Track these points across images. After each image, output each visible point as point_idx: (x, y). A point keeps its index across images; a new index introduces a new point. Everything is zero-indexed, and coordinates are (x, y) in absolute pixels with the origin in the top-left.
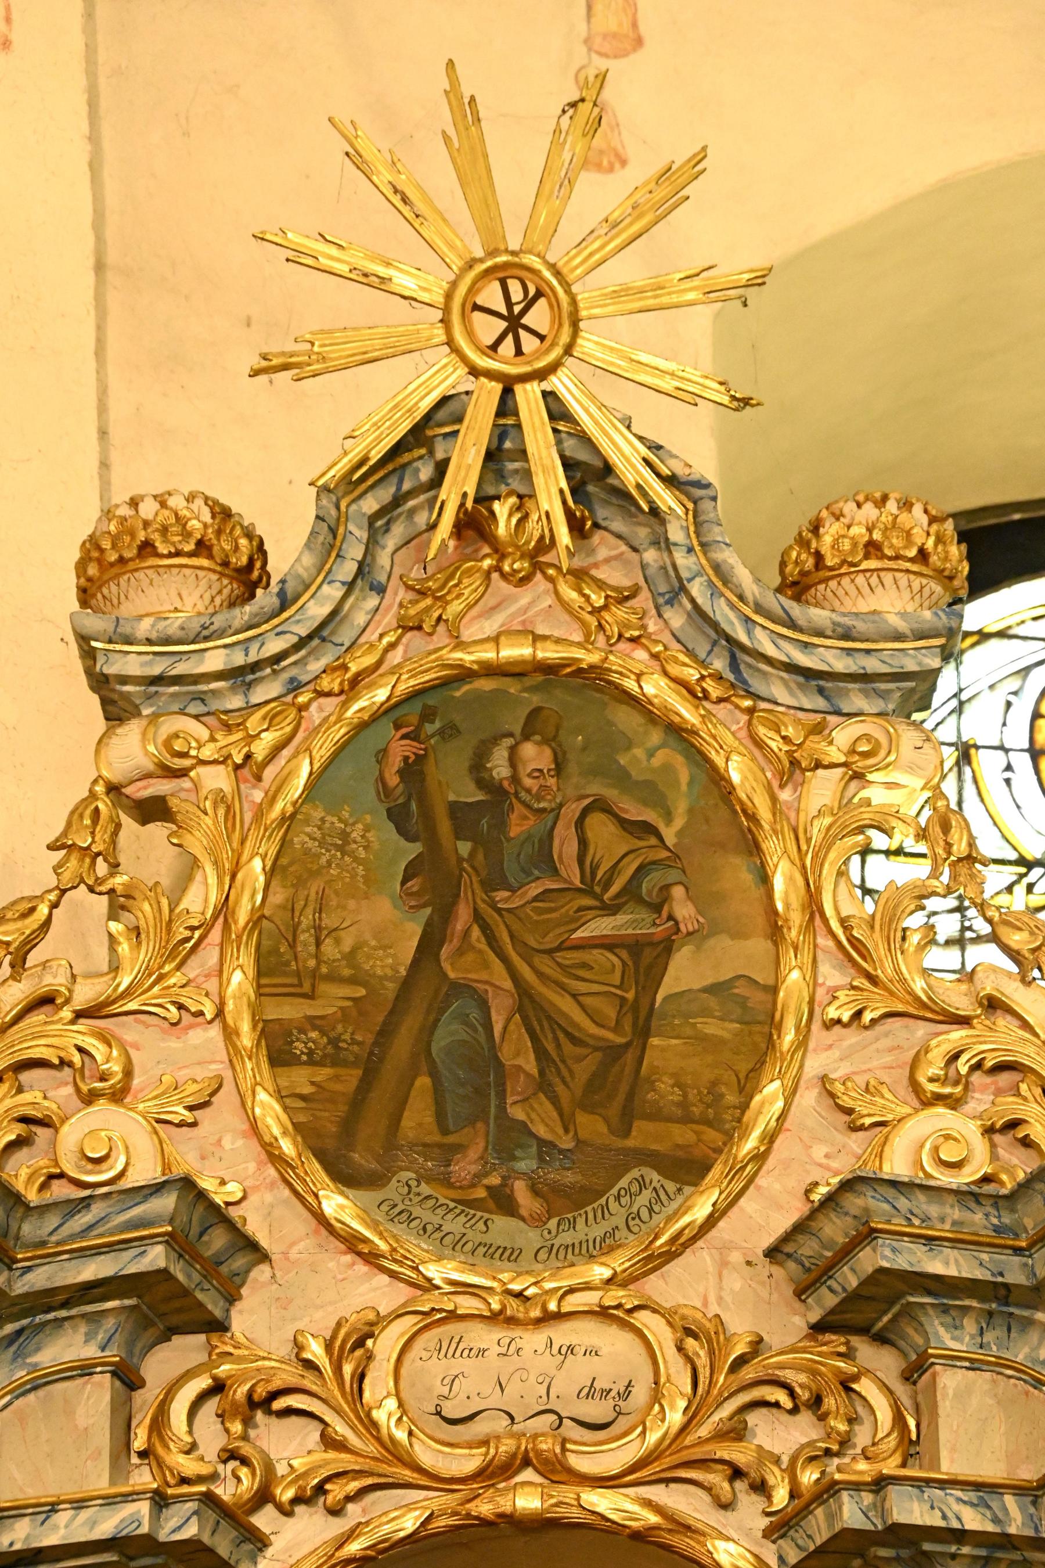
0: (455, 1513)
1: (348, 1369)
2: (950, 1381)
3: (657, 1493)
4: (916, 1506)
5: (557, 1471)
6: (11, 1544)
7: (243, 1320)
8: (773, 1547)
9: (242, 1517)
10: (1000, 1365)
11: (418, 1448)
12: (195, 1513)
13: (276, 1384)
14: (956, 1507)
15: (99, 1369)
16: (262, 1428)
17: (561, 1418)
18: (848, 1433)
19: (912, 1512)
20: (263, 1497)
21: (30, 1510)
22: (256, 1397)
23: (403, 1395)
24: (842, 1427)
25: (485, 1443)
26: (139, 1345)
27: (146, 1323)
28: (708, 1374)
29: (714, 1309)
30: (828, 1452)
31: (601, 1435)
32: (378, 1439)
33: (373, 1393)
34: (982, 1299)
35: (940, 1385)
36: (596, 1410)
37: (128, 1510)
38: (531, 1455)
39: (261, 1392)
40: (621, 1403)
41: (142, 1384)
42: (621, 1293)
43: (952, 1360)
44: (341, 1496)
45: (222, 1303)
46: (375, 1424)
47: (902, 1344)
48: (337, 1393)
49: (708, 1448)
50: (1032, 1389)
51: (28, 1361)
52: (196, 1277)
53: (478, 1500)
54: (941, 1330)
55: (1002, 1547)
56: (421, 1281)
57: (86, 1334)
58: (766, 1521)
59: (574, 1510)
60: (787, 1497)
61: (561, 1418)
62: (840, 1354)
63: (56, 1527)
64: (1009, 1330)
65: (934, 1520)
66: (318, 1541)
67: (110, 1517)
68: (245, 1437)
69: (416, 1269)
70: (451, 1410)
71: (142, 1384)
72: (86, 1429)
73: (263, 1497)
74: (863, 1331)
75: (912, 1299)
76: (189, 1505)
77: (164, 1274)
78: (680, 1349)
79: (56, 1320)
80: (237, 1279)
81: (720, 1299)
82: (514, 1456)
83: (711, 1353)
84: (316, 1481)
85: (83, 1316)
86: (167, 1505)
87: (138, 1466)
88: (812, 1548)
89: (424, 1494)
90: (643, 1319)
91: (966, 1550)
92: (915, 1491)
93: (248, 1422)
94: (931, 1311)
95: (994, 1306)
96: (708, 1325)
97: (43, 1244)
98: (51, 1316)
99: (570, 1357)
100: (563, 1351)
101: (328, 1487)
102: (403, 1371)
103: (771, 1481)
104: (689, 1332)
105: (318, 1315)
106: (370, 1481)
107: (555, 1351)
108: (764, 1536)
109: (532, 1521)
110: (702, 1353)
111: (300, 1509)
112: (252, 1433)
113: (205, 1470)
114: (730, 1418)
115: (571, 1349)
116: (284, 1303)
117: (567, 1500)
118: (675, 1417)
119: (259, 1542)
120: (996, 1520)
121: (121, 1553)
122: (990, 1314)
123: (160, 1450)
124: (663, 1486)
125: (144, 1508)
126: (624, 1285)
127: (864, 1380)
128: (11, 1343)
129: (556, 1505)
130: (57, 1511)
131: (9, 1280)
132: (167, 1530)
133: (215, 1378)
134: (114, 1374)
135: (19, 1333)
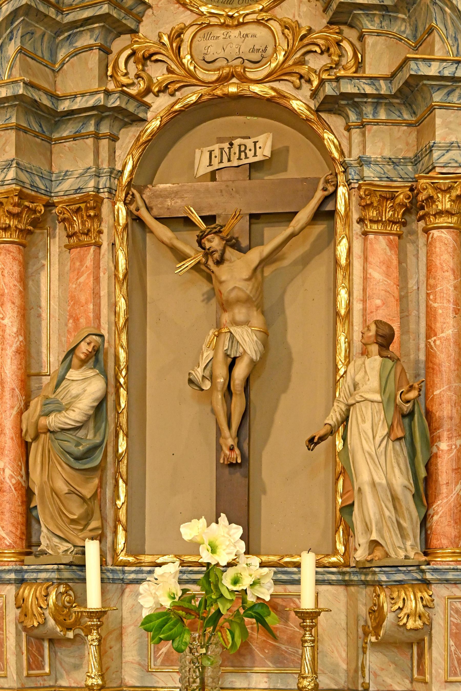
0: (209, 94)
1: (174, 45)
2: (370, 40)
3: (276, 85)
4: (349, 86)
5: (243, 79)
7: (144, 30)
8: (313, 101)
10: (386, 35)
11: (197, 72)
12: (119, 97)
13: (152, 51)
14: (363, 86)
16: (149, 67)
17: (244, 60)
18: (339, 61)
20: (148, 91)
22: (145, 56)
23: (193, 54)
24: (336, 59)
26: (109, 39)
27: (109, 31)
30: (331, 68)
31: (257, 65)
34: (380, 11)
36: (255, 57)
37: (97, 96)
39: (147, 54)
41: (111, 52)
42: (264, 14)
43: (371, 33)
44: (173, 90)
48: (171, 53)
49: (291, 68)
52: (123, 15)
54: (367, 22)
56: (200, 13)
61: (244, 60)
62: (337, 33)
63: (76, 103)
64: (390, 21)
65: (356, 91)
68: (143, 70)
69: (198, 8)
70: (208, 59)
71: (111, 52)
73: (148, 91)
74: (345, 24)
75: (355, 12)
77: (108, 14)
80: (140, 15)
81: (299, 14)
82: (228, 74)
83: (293, 34)
85: (88, 29)
86: (110, 95)
87: (110, 81)
89: (201, 88)
90: (272, 24)
91: (370, 100)
92: (349, 81)
93: (144, 65)
94: (363, 16)
95: (384, 13)
96: (293, 24)
97: (71, 5)
98: (78, 30)
99: (247, 38)
101: (169, 86)
102: (193, 45)
103: (312, 79)
104: (286, 28)
105: (167, 26)
106: (182, 84)
109: (235, 96)
110: (290, 35)
111: (161, 94)
112: (146, 68)
113: (130, 81)
114: (299, 57)
115: (247, 35)
116: (156, 22)
118: (281, 58)
119: (148, 106)
120: (377, 89)
121: (98, 111)
122: (383, 16)
123: (115, 75)
125: (102, 96)
126: (266, 12)
127: (344, 41)
128: (68, 39)
129: (242, 90)
131: (62, 18)
133: (132, 50)
134: (99, 49)
135: (69, 36)
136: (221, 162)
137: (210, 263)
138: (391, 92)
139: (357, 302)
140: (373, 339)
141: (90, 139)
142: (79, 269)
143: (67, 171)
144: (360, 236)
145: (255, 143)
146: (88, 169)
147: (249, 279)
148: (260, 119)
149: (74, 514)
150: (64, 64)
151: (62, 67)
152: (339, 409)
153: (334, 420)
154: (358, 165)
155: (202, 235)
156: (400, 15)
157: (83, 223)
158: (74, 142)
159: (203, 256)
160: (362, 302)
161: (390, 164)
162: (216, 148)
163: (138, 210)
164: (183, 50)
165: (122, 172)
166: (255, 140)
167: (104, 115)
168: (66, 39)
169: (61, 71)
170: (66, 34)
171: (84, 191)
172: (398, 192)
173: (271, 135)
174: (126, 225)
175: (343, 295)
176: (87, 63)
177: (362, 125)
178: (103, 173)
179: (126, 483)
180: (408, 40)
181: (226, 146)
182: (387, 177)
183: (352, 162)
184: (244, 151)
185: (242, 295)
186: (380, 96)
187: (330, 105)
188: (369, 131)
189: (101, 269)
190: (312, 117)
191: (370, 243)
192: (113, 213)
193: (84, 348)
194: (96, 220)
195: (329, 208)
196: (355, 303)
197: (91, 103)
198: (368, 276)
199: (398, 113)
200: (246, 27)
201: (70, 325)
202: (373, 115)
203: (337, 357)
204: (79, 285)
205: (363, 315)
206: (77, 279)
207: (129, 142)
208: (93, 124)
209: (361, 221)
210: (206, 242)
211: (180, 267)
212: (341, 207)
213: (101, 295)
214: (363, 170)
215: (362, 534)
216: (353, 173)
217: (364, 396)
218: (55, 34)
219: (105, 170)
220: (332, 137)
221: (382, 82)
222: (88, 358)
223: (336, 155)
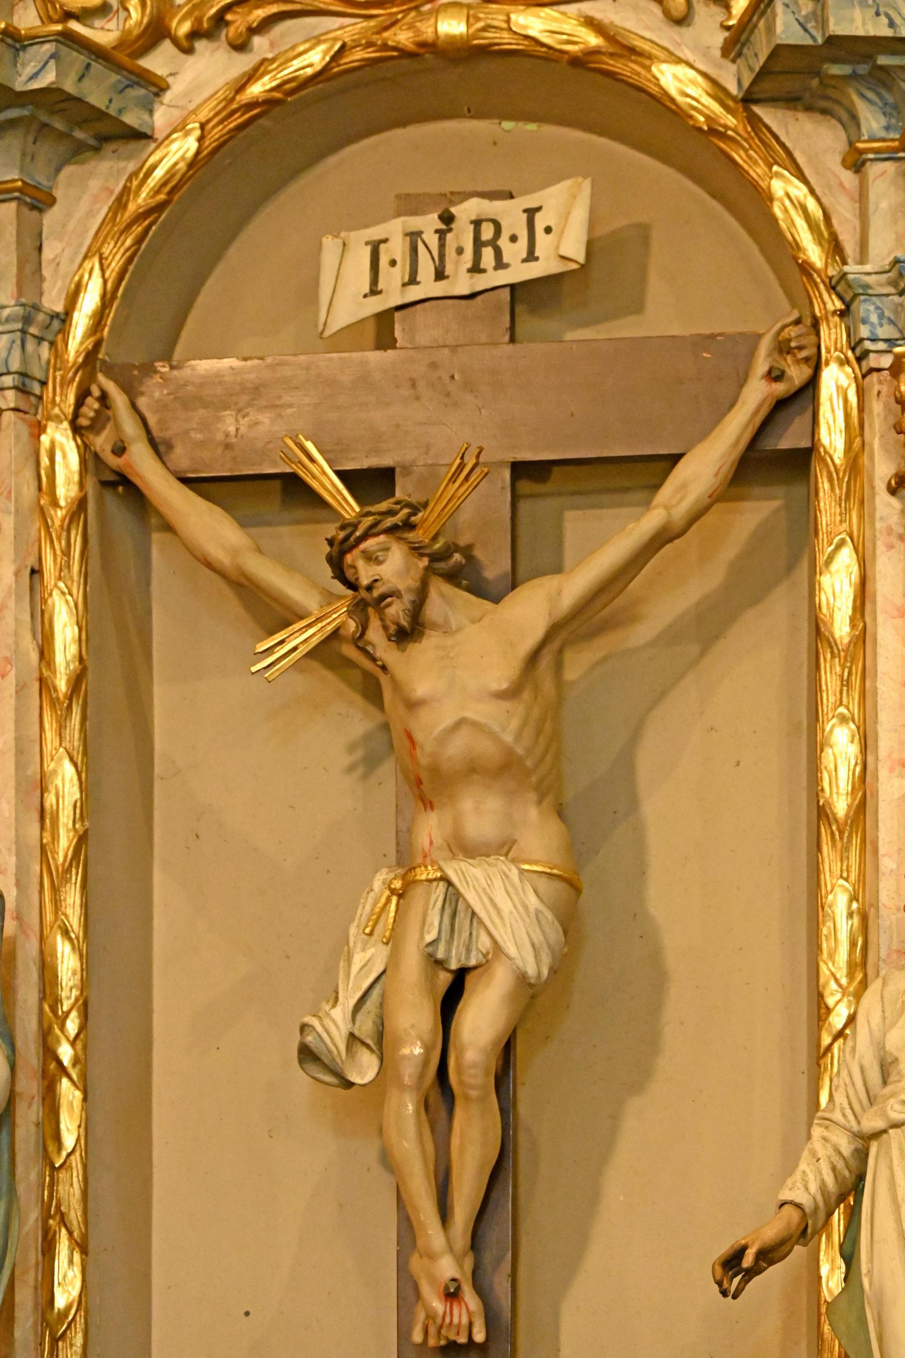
0: (370, 44)
4: (857, 13)
8: (733, 68)
12: (53, 56)
19: (852, 20)
44: (242, 29)
53: (398, 26)
59: (505, 35)
66: (220, 82)
73: (156, 32)
76: (47, 46)
84: (213, 11)
86: (24, 48)
101: (229, 17)
111: (201, 45)
117: (496, 23)
129: (484, 29)
132: (24, 78)
136: (413, 280)
137: (375, 635)
139: (892, 770)
145: (531, 212)
148: (550, 130)
152: (830, 1151)
153: (813, 1187)
155: (346, 538)
159: (349, 613)
162: (394, 230)
163: (120, 450)
165: (65, 318)
166: (530, 201)
173: (587, 185)
174: (81, 505)
181: (429, 223)
183: (869, 279)
184: (493, 243)
185: (485, 747)
195: (789, 439)
196: (883, 773)
203: (823, 967)
207: (90, 214)
210: (361, 564)
212: (832, 437)
216: (874, 318)
223: (814, 254)
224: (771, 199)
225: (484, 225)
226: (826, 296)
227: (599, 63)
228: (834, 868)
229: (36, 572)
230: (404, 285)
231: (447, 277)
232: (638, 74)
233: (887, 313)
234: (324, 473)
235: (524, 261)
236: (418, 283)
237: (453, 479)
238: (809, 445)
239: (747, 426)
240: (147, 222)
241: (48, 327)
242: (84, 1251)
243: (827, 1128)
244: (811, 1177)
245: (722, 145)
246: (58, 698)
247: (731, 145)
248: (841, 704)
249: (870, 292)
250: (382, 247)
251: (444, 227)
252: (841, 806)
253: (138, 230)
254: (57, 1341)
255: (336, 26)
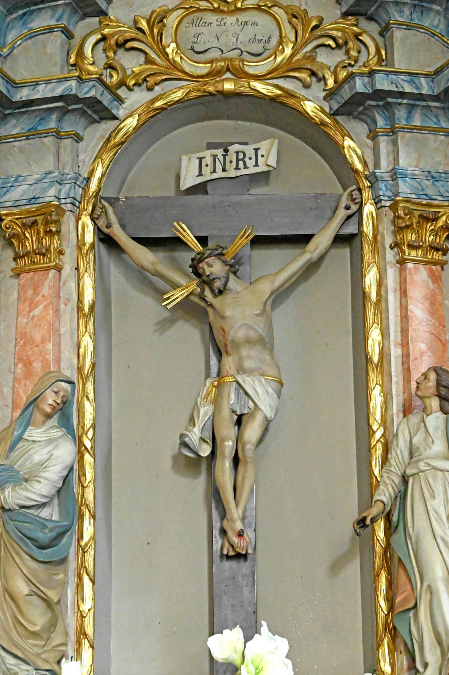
0: (199, 90)
1: (155, 31)
2: (398, 34)
5: (240, 74)
6: (21, 98)
9: (113, 90)
15: (56, 30)
17: (242, 51)
18: (358, 57)
20: (122, 83)
21: (28, 84)
22: (119, 42)
23: (178, 42)
25: (211, 62)
28: (301, 33)
29: (304, 7)
32: (168, 60)
33: (166, 41)
35: (395, 36)
36: (256, 48)
37: (67, 84)
38: (230, 66)
39: (121, 40)
40: (266, 45)
45: (105, 3)
46: (167, 54)
47: (379, 20)
48: (151, 41)
50: (431, 38)
51: (28, 26)
53: (209, 84)
54: (395, 13)
55: (419, 100)
57: (51, 15)
58: (324, 94)
60: (333, 83)
61: (242, 51)
63: (38, 91)
66: (144, 101)
67: (60, 87)
70: (198, 48)
72: (51, 54)
78: (290, 23)
79: (39, 9)
83: (303, 24)
84: (143, 77)
85: (49, 7)
86: (83, 83)
88: (343, 102)
91: (405, 101)
94: (391, 5)
95: (416, 2)
96: (302, 13)
99: (246, 26)
100: (243, 23)
101: (148, 79)
102: (178, 32)
103: (327, 76)
105: (144, 10)
106: (165, 77)
107: (240, 23)
108: (324, 100)
111: (136, 88)
115: (246, 23)
118: (288, 51)
119: (121, 101)
120: (417, 88)
122: (415, 6)
123: (81, 64)
124: (283, 79)
127: (364, 35)
128: (21, 19)
130: (39, 85)
132: (83, 93)
135: (24, 14)
136: (214, 171)
137: (208, 293)
138: (433, 92)
139: (395, 346)
140: (433, 390)
141: (48, 138)
142: (32, 300)
143: (19, 176)
144: (395, 265)
145: (256, 150)
146: (48, 174)
147: (261, 315)
148: (255, 125)
149: (35, 624)
150: (14, 48)
151: (11, 52)
153: (387, 495)
154: (390, 179)
155: (200, 258)
156: (435, 7)
157: (39, 240)
158: (27, 141)
159: (198, 285)
160: (400, 347)
161: (429, 178)
162: (208, 154)
163: (109, 226)
164: (166, 37)
165: (88, 180)
166: (256, 146)
167: (70, 108)
168: (19, 18)
169: (9, 57)
170: (21, 12)
171: (41, 200)
172: (439, 212)
173: (276, 141)
174: (93, 245)
175: (374, 336)
176: (45, 47)
177: (392, 132)
178: (66, 180)
179: (93, 582)
180: (442, 36)
181: (220, 152)
182: (426, 195)
183: (382, 175)
184: (243, 160)
185: (253, 335)
186: (419, 96)
187: (353, 107)
188: (402, 138)
189: (61, 299)
190: (328, 120)
191: (409, 274)
192: (76, 229)
193: (50, 399)
194: (56, 238)
195: (351, 229)
196: (392, 347)
197: (59, 91)
198: (409, 313)
199: (435, 120)
200: (245, 14)
201: (19, 371)
202: (407, 120)
204: (33, 319)
205: (403, 364)
206: (30, 311)
207: (97, 145)
208: (54, 120)
209: (396, 245)
210: (206, 267)
211: (168, 298)
212: (368, 228)
213: (61, 333)
214: (397, 185)
215: (431, 649)
216: (384, 188)
217: (431, 463)
218: (7, 11)
219: (69, 176)
220: (352, 144)
221: (422, 79)
222: (54, 412)
223: (359, 166)
224: (344, 148)
225: (240, 154)
226: (364, 181)
227: (281, 100)
228: (374, 380)
229: (77, 269)
230: (211, 173)
231: (227, 171)
232: (295, 104)
233: (389, 187)
234: (189, 235)
235: (254, 166)
236: (216, 172)
237: (241, 238)
238: (356, 232)
239: (338, 225)
240: (118, 148)
241: (82, 183)
242: (94, 519)
243: (388, 473)
244: (386, 491)
245: (325, 129)
246: (85, 314)
247: (328, 128)
248: (374, 323)
249: (383, 179)
250: (203, 159)
251: (225, 153)
252: (376, 359)
253: (115, 150)
254: (84, 553)
255: (186, 84)
